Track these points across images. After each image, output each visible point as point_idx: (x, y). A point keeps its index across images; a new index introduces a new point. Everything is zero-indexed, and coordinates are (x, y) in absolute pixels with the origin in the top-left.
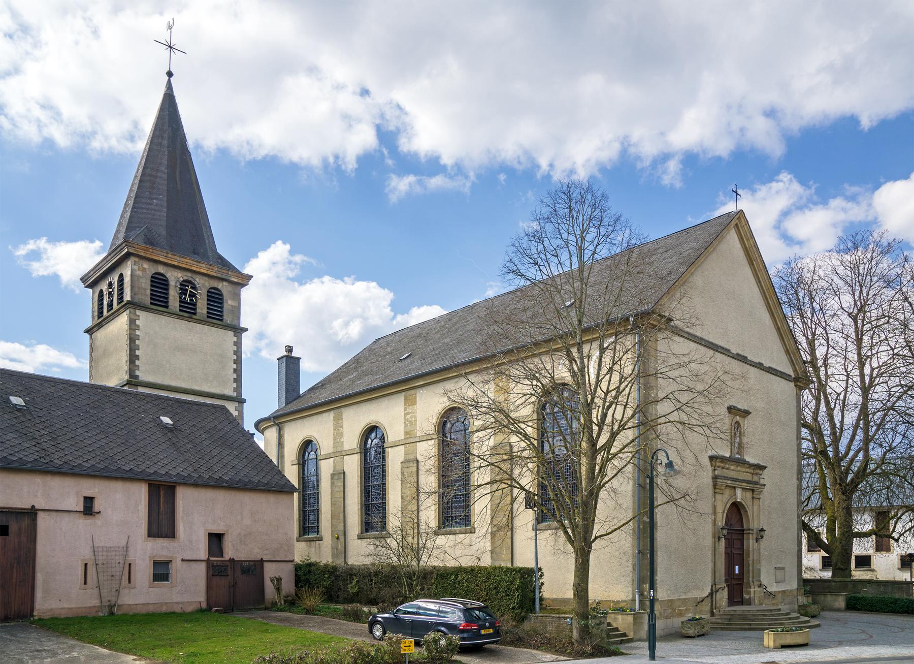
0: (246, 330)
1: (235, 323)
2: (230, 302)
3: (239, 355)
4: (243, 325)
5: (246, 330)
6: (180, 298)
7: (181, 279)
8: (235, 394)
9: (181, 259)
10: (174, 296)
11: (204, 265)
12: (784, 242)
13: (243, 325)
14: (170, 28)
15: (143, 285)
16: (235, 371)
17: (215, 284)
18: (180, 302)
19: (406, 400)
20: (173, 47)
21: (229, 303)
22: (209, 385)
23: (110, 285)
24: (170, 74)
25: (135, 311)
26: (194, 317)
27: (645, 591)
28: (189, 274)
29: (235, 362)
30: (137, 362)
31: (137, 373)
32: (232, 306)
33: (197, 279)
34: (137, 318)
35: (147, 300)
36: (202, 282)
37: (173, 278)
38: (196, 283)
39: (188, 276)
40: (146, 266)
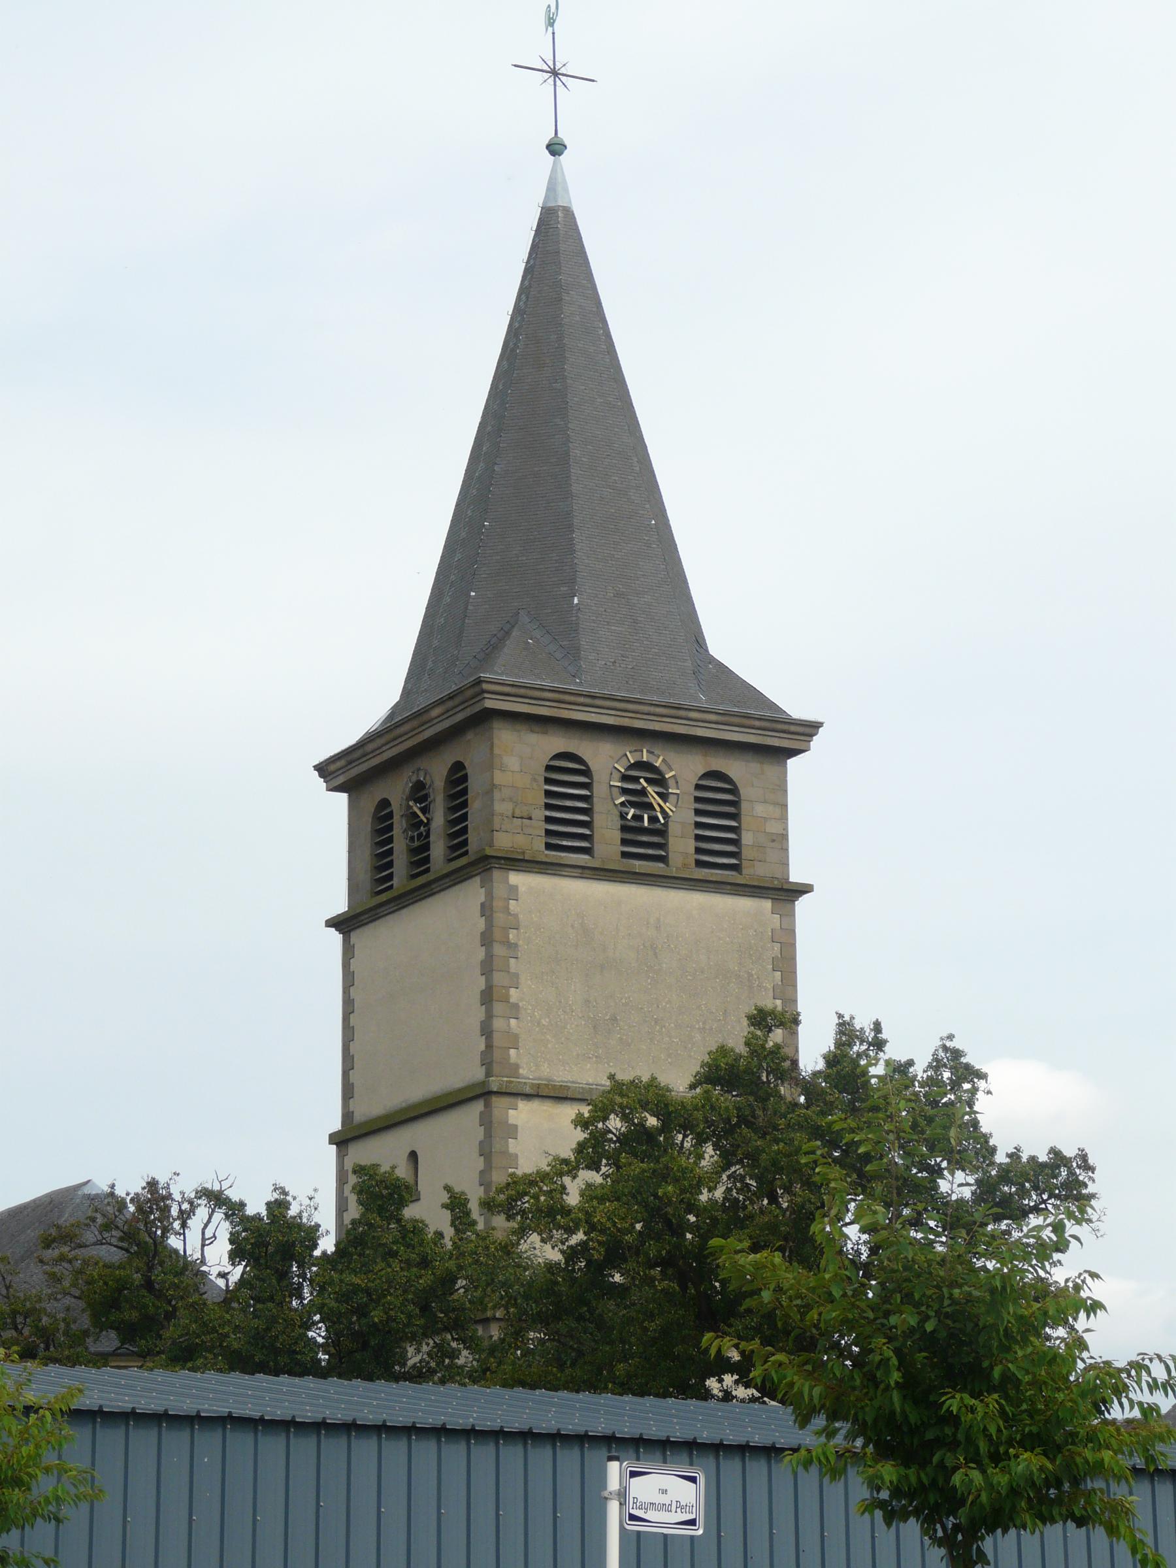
0: (805, 889)
5: (805, 889)
6: (623, 816)
12: (900, 1061)
13: (796, 876)
14: (551, 22)
18: (624, 829)
19: (485, 1100)
21: (754, 810)
23: (419, 792)
24: (555, 148)
27: (1027, 1226)
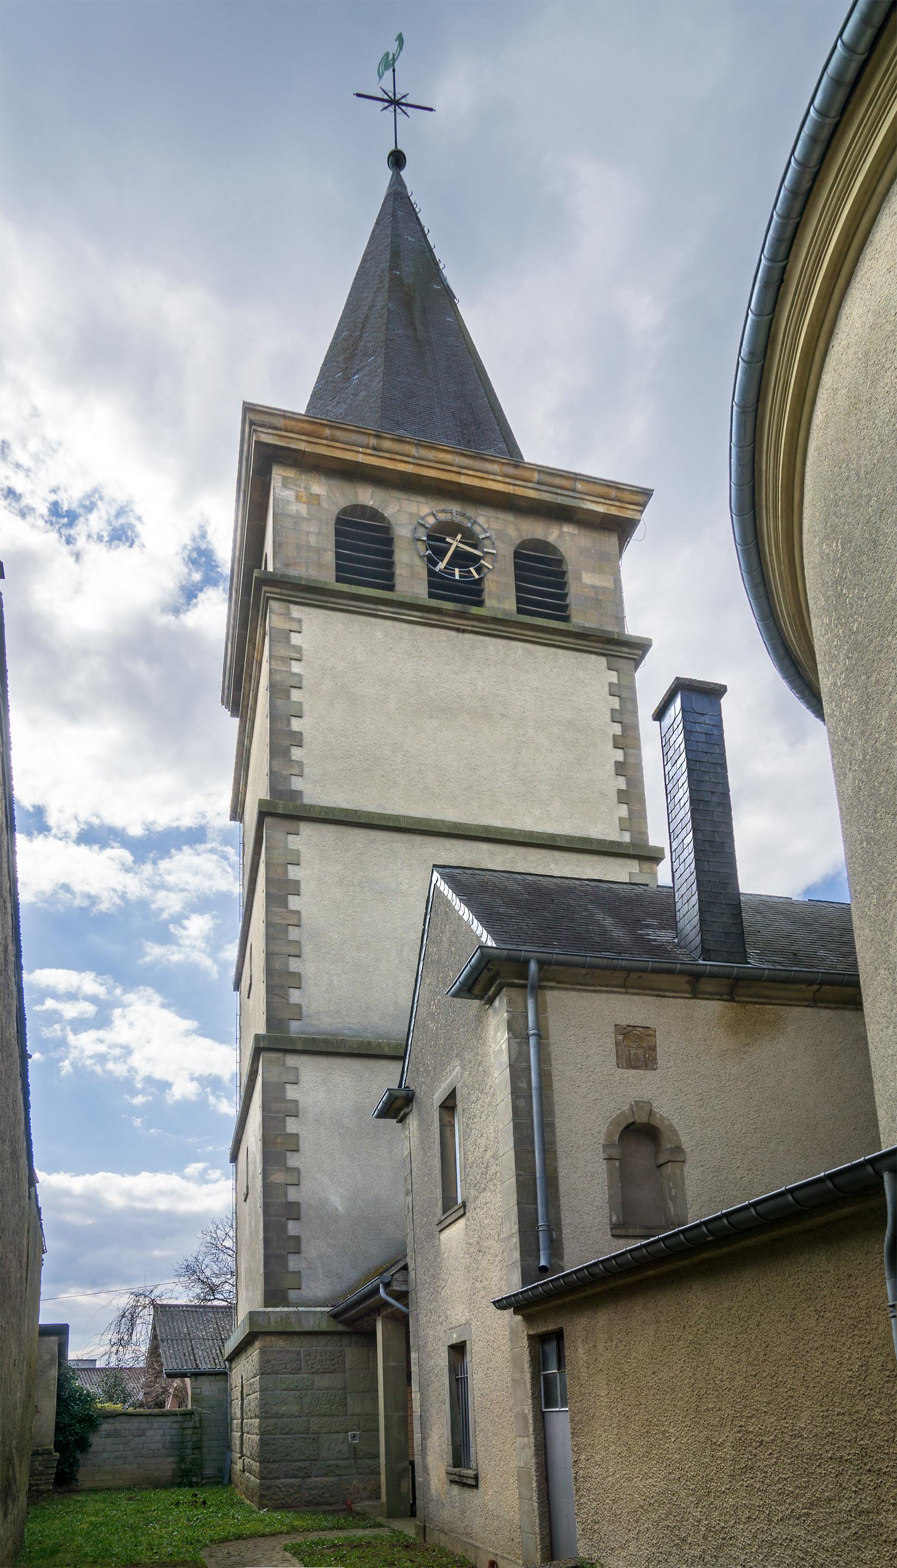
0: (501, 1304)
1: (610, 627)
2: (588, 578)
3: (627, 719)
4: (633, 628)
5: (501, 1304)
7: (431, 521)
8: (626, 838)
9: (424, 452)
10: (411, 567)
11: (495, 468)
15: (313, 540)
16: (620, 768)
17: (536, 530)
20: (403, 101)
22: (538, 812)
24: (397, 160)
25: (289, 609)
26: (475, 610)
28: (455, 507)
29: (618, 743)
30: (296, 753)
31: (297, 784)
32: (593, 587)
33: (481, 520)
34: (294, 626)
35: (327, 576)
36: (494, 525)
37: (404, 518)
38: (477, 529)
39: (452, 511)
40: (319, 487)
